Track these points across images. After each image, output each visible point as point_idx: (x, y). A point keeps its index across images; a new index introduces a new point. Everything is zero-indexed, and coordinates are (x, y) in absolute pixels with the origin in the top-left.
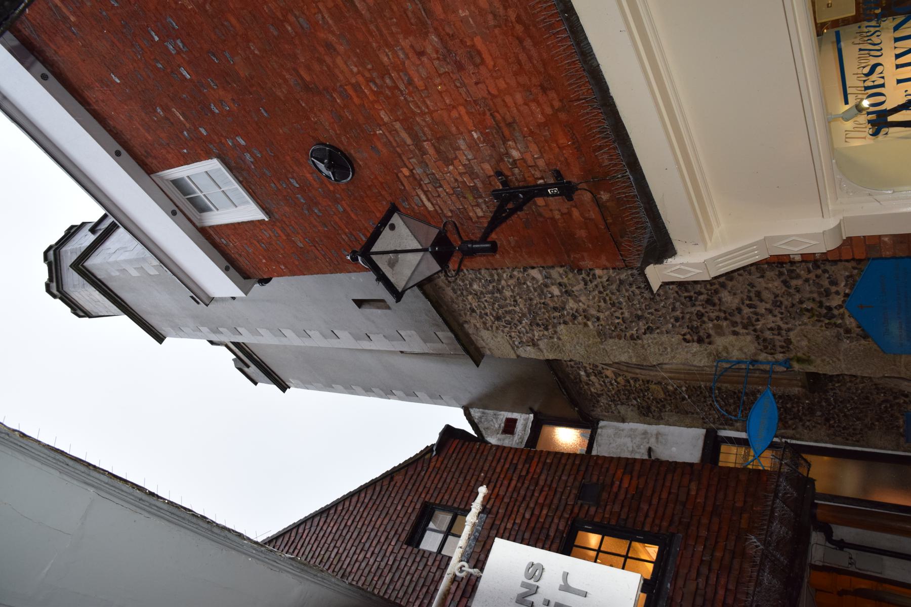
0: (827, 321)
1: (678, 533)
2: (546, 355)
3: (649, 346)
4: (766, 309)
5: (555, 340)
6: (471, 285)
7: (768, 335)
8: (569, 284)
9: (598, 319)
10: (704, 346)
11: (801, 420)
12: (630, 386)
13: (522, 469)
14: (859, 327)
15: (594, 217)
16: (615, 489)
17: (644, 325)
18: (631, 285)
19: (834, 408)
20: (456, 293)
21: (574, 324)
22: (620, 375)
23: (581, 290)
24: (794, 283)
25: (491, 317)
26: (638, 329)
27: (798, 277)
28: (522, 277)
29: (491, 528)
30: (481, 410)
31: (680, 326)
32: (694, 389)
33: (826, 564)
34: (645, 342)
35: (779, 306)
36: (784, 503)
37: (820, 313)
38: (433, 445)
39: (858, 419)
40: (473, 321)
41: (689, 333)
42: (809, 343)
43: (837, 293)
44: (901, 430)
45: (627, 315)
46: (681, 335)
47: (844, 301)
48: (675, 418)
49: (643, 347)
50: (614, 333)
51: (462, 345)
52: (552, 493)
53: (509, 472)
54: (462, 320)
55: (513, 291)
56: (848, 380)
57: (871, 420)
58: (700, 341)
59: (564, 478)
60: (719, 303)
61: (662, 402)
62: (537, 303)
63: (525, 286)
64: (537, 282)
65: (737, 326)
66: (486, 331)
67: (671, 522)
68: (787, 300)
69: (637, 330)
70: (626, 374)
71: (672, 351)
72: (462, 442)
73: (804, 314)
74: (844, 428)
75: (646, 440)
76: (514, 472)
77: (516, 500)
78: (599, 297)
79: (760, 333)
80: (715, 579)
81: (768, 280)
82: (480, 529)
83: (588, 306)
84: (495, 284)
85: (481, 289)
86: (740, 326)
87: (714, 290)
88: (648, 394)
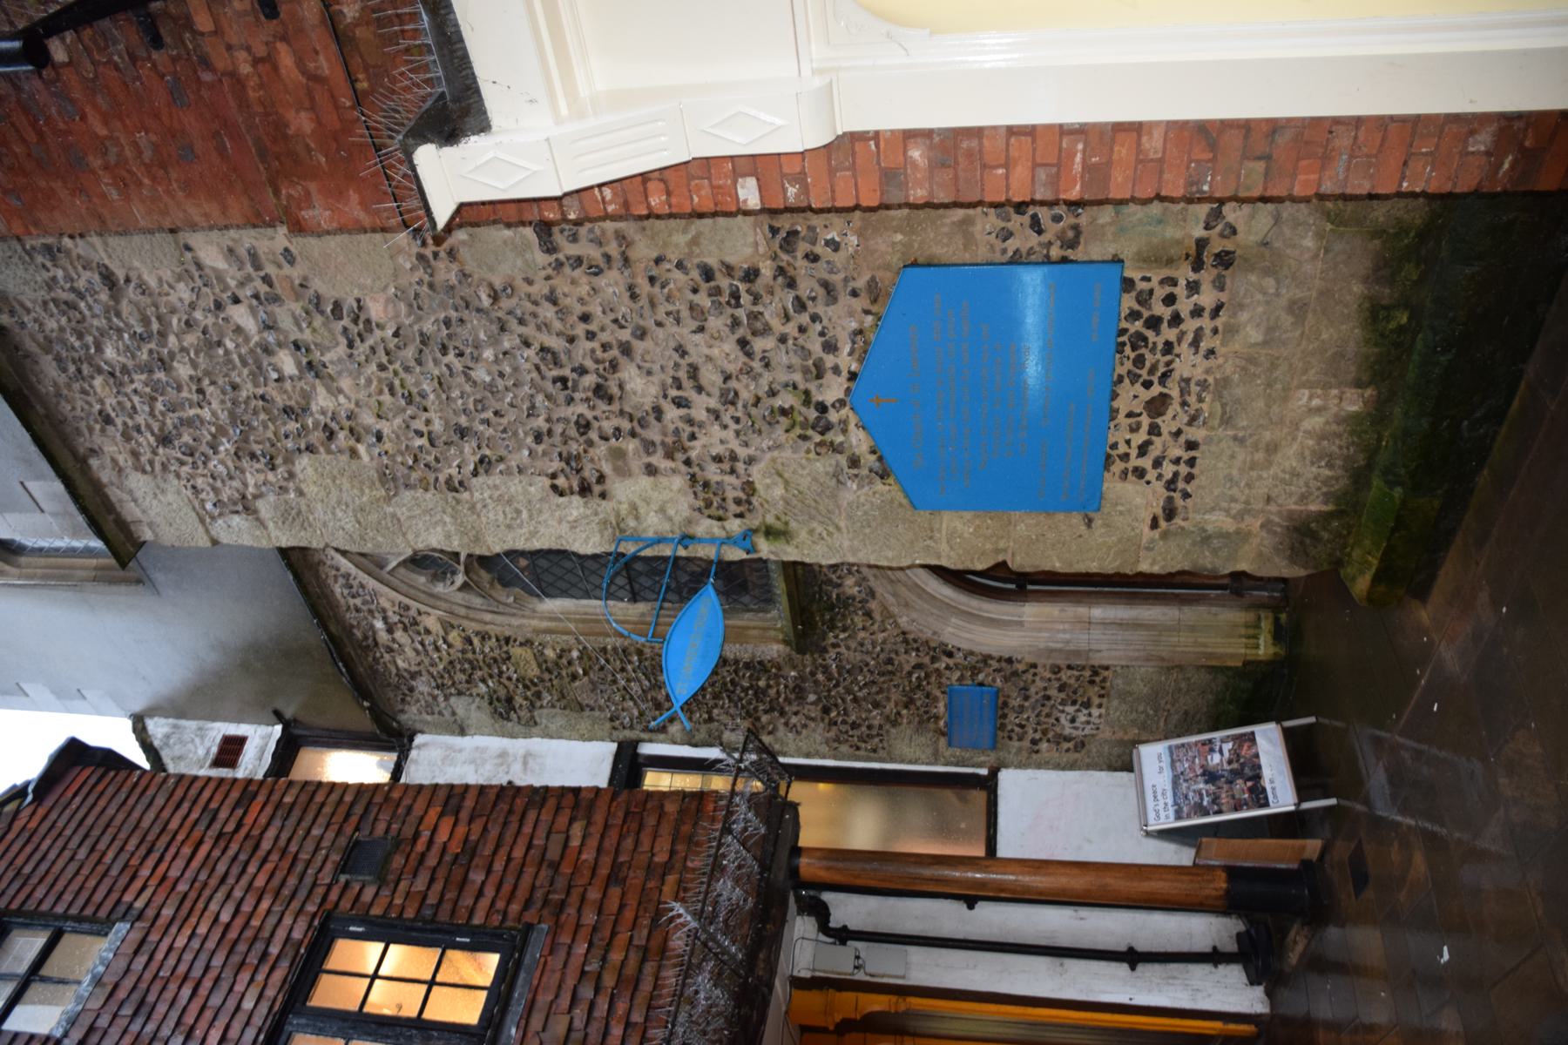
0: (818, 438)
1: (539, 922)
2: (273, 535)
3: (485, 506)
4: (708, 410)
5: (292, 495)
6: (99, 349)
7: (713, 473)
8: (316, 345)
9: (379, 437)
10: (595, 502)
11: (782, 713)
12: (474, 652)
13: (227, 820)
14: (873, 452)
15: (327, 72)
16: (420, 846)
17: (474, 453)
18: (444, 350)
19: (836, 686)
20: (64, 370)
21: (329, 452)
22: (452, 627)
23: (340, 361)
24: (759, 344)
25: (149, 435)
26: (463, 461)
27: (767, 330)
28: (214, 324)
29: (136, 952)
30: (171, 721)
31: (545, 453)
33: (818, 974)
34: (477, 495)
35: (733, 403)
36: (743, 844)
37: (806, 419)
38: (27, 784)
39: (876, 705)
40: (109, 448)
41: (562, 471)
42: (787, 490)
43: (836, 370)
44: (942, 723)
45: (437, 426)
46: (547, 475)
47: (848, 391)
48: (560, 721)
49: (472, 508)
50: (415, 476)
51: (83, 510)
52: (286, 864)
53: (197, 828)
54: (82, 444)
55: (194, 365)
56: (860, 626)
57: (896, 705)
58: (585, 490)
59: (316, 832)
60: (619, 394)
61: (535, 685)
62: (248, 398)
63: (221, 351)
64: (247, 339)
65: (655, 452)
66: (139, 475)
67: (527, 904)
68: (747, 386)
70: (465, 623)
71: (531, 517)
72: (101, 771)
73: (778, 422)
74: (854, 726)
75: (504, 767)
76: (208, 827)
77: (205, 884)
78: (380, 380)
79: (696, 469)
80: (606, 1006)
81: (712, 337)
82: (111, 955)
83: (357, 404)
84: (153, 346)
85: (122, 359)
86: (660, 452)
87: (611, 361)
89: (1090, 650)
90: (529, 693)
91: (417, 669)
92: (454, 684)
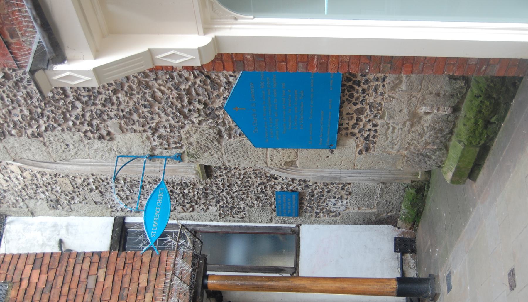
7: (226, 122)
12: (38, 180)
32: (101, 181)
39: (242, 199)
58: (101, 137)
61: (71, 194)
69: (37, 128)
70: (33, 168)
88: (56, 187)
89: (341, 177)
90: (68, 198)
91: (7, 188)
92: (27, 194)
